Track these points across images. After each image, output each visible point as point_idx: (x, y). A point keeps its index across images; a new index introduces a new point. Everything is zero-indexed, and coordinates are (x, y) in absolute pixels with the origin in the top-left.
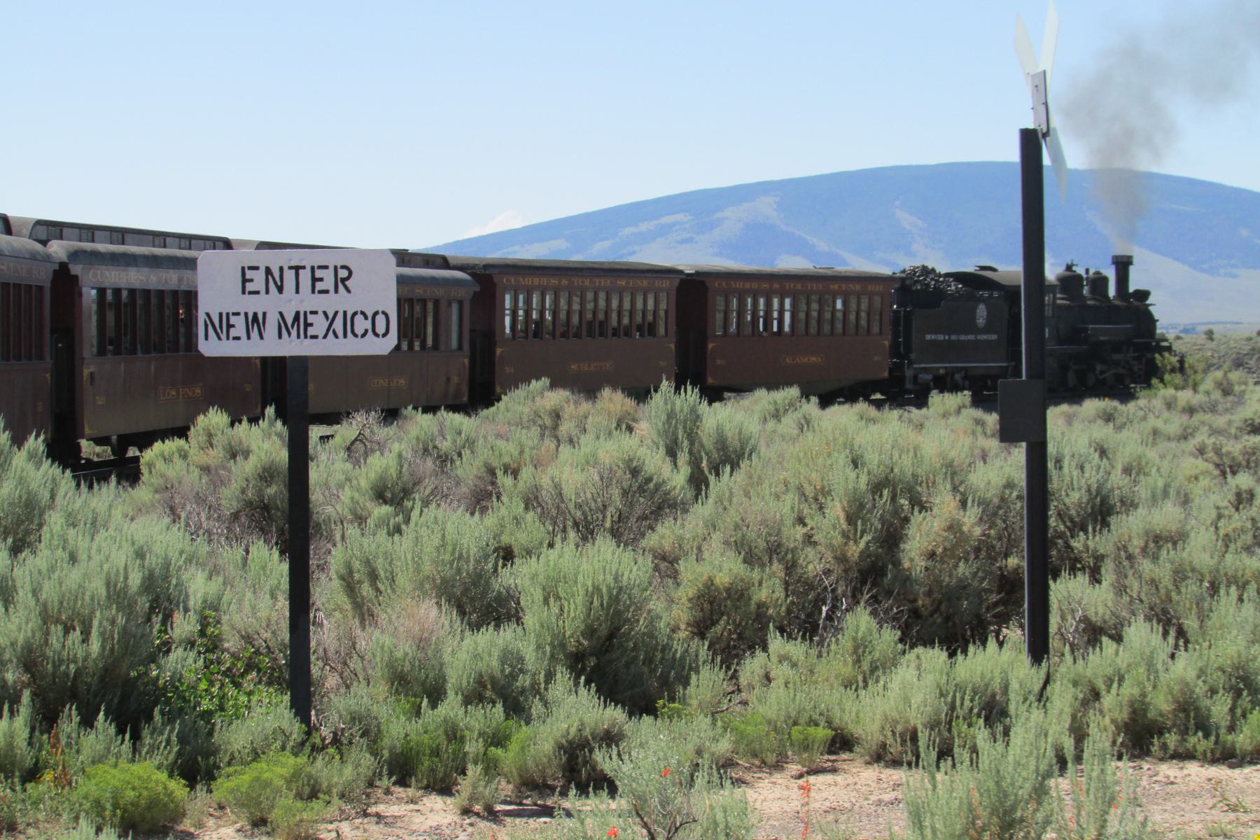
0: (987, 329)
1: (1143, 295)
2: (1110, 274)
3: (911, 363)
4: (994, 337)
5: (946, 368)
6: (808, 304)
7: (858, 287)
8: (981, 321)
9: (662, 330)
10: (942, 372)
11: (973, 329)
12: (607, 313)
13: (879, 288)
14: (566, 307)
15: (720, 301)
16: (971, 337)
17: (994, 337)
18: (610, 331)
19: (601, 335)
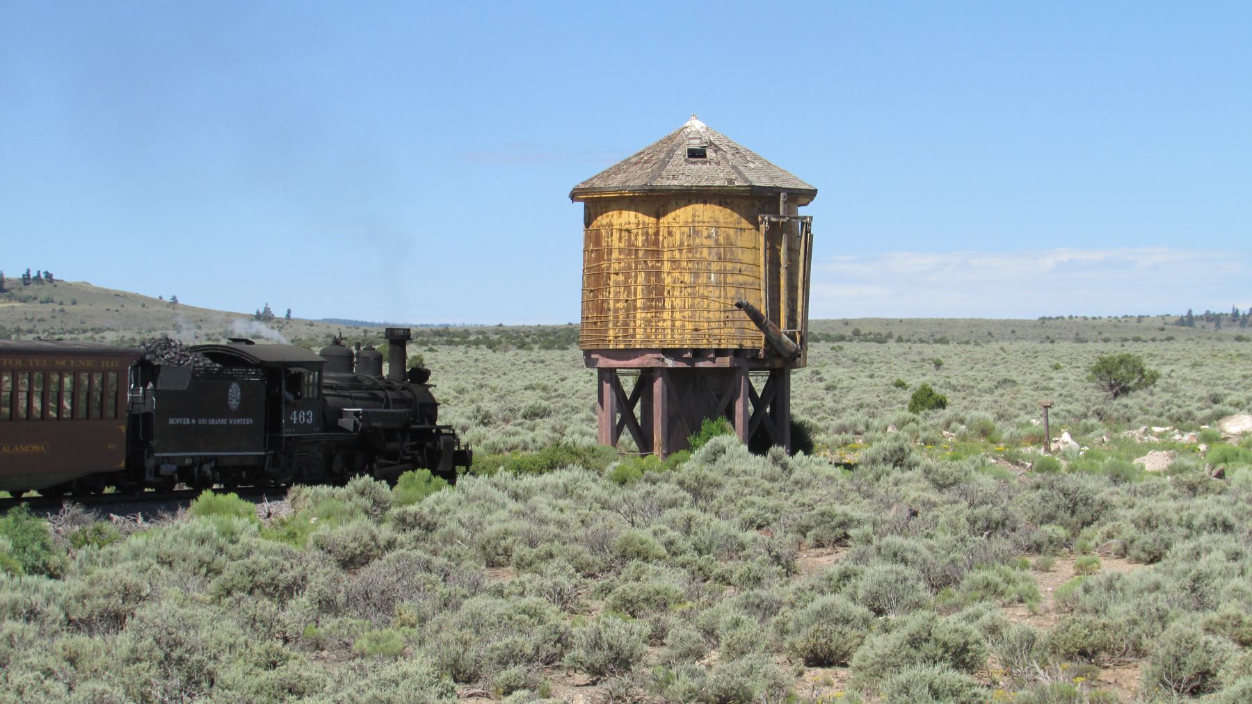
0: (241, 412)
4: (249, 421)
8: (234, 403)
10: (188, 462)
11: (224, 411)
16: (224, 421)
17: (249, 421)
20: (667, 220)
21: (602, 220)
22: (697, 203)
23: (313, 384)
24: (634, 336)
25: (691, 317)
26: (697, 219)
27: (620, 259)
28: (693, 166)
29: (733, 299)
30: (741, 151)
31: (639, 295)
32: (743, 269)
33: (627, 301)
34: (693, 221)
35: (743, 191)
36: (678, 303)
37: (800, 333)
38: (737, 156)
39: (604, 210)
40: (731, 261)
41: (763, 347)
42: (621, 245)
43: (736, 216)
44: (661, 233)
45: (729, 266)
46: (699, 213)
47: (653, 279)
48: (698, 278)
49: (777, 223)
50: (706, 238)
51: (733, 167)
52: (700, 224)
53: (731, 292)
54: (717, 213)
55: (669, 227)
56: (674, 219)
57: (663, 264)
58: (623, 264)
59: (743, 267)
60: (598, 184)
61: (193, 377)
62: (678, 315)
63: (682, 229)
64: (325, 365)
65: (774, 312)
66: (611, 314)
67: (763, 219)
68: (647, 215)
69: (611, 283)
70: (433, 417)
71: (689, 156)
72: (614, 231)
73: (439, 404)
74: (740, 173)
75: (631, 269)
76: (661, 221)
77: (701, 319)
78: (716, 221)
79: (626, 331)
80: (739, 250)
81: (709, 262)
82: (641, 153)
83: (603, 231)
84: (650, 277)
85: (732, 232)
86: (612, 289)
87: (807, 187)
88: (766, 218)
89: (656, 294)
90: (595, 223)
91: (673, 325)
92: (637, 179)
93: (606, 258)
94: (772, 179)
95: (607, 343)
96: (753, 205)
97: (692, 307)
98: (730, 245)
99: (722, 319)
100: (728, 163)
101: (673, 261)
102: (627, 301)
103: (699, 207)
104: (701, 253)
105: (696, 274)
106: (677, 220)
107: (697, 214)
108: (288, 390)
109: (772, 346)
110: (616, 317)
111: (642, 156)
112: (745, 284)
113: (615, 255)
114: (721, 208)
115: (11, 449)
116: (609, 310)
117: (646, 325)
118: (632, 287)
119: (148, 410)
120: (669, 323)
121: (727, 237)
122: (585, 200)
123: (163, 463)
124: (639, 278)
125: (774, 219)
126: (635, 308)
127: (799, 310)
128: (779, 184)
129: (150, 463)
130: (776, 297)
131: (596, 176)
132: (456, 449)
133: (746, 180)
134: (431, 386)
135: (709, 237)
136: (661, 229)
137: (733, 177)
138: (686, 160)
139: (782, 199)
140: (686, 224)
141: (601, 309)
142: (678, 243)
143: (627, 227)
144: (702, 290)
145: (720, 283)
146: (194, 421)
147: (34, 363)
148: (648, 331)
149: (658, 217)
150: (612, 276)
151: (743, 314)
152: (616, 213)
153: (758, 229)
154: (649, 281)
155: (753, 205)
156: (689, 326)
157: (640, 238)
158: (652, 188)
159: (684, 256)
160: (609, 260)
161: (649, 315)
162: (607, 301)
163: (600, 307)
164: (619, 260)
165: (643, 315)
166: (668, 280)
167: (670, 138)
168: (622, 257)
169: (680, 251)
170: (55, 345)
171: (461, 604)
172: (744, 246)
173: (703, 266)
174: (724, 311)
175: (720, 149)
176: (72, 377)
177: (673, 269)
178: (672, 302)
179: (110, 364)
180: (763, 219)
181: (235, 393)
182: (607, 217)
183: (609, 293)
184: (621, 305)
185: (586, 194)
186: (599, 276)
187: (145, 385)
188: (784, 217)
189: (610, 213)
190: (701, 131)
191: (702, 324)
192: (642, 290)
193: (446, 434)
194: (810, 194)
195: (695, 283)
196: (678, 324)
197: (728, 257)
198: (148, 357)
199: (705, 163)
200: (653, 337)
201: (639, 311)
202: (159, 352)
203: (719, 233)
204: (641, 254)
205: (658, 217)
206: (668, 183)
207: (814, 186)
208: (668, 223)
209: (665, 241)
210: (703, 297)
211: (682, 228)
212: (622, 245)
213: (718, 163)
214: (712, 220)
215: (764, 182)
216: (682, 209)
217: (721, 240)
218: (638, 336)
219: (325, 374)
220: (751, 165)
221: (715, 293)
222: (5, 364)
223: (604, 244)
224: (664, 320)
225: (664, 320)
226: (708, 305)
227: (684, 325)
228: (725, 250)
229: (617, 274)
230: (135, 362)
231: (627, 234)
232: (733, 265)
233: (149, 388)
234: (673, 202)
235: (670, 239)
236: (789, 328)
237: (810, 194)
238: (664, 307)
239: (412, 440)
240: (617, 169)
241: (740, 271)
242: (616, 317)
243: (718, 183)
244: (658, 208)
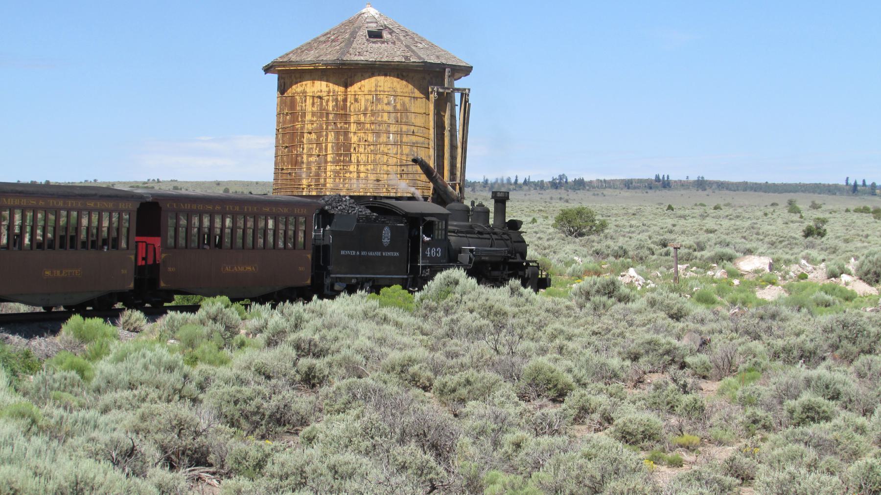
0: (391, 248)
1: (515, 225)
2: (490, 205)
3: (329, 273)
4: (396, 254)
5: (357, 278)
6: (286, 225)
7: (286, 210)
8: (386, 241)
9: (124, 245)
10: (353, 281)
11: (379, 247)
12: (118, 230)
13: (304, 211)
14: (197, 224)
15: (171, 222)
16: (379, 254)
17: (396, 254)
18: (79, 245)
19: (72, 247)
20: (355, 88)
21: (297, 88)
22: (379, 75)
23: (442, 230)
24: (325, 185)
25: (374, 170)
26: (379, 89)
27: (313, 121)
28: (374, 45)
29: (407, 155)
30: (409, 33)
31: (330, 151)
32: (415, 131)
33: (319, 156)
34: (376, 91)
35: (417, 66)
36: (363, 158)
37: (459, 184)
38: (408, 37)
39: (299, 80)
40: (407, 124)
41: (431, 196)
42: (314, 109)
43: (411, 87)
44: (349, 100)
45: (405, 128)
46: (381, 84)
47: (342, 138)
48: (380, 137)
49: (443, 93)
50: (386, 104)
51: (407, 46)
52: (382, 93)
53: (406, 150)
54: (395, 84)
55: (355, 95)
56: (360, 88)
57: (350, 125)
58: (315, 125)
59: (416, 129)
60: (294, 58)
61: (358, 221)
62: (362, 168)
63: (367, 97)
64: (450, 216)
65: (440, 166)
66: (305, 166)
67: (433, 90)
68: (336, 84)
69: (305, 141)
70: (523, 254)
71: (370, 37)
72: (308, 97)
73: (528, 245)
74: (413, 51)
75: (322, 129)
76: (349, 90)
77: (382, 172)
78: (394, 91)
79: (318, 180)
80: (413, 115)
81: (389, 125)
82: (327, 34)
83: (298, 98)
84: (338, 137)
85: (407, 100)
86: (305, 146)
87: (464, 64)
88: (435, 89)
89: (344, 150)
90: (290, 90)
91: (358, 177)
92: (329, 55)
93: (300, 120)
94: (438, 57)
95: (301, 190)
96: (424, 78)
97: (374, 162)
98: (405, 111)
99: (399, 172)
100: (402, 43)
101: (358, 123)
102: (319, 156)
103: (381, 79)
104: (382, 117)
105: (377, 134)
106: (363, 89)
107: (379, 84)
108: (424, 233)
109: (439, 195)
110: (309, 169)
111: (329, 36)
112: (417, 143)
113: (308, 117)
114: (399, 80)
115: (231, 269)
116: (303, 163)
117: (335, 176)
118: (324, 145)
119: (326, 242)
120: (355, 175)
121: (403, 104)
122: (279, 72)
123: (337, 282)
124: (330, 137)
125: (441, 90)
126: (326, 162)
127: (459, 165)
128: (444, 62)
129: (327, 281)
130: (441, 154)
131: (292, 52)
132: (540, 276)
133: (419, 57)
134: (523, 232)
135: (388, 104)
136: (349, 96)
137: (408, 54)
138: (367, 40)
139: (446, 74)
140: (370, 93)
141: (296, 162)
142: (363, 108)
143: (319, 94)
144: (383, 148)
145: (397, 142)
146: (358, 253)
147: (248, 209)
148: (337, 180)
149: (346, 86)
150: (305, 135)
151: (418, 168)
152: (309, 83)
153: (428, 98)
154: (338, 139)
155: (424, 78)
156: (372, 177)
157: (331, 104)
158: (343, 62)
159: (368, 119)
160: (303, 121)
161: (338, 168)
162: (301, 155)
163: (294, 160)
164: (312, 122)
165: (333, 168)
166: (354, 139)
167: (351, 22)
168: (315, 119)
169: (365, 114)
170: (263, 197)
171: (110, 410)
172: (418, 112)
173: (383, 127)
174: (401, 165)
175: (393, 32)
176: (44, 212)
177: (359, 130)
178: (358, 157)
179: (300, 211)
180: (433, 90)
181: (387, 233)
182: (301, 86)
183: (303, 149)
184: (312, 159)
185: (284, 66)
186: (293, 135)
187: (324, 227)
188: (448, 89)
189: (304, 83)
190: (376, 16)
191: (382, 176)
192: (332, 147)
193: (533, 266)
194: (466, 70)
195: (376, 141)
196: (362, 175)
197: (404, 121)
198: (327, 208)
199: (383, 42)
200: (341, 186)
201: (329, 164)
202: (334, 204)
203: (397, 100)
204: (331, 117)
205: (346, 86)
206: (356, 58)
207: (470, 64)
208: (355, 92)
209: (352, 107)
210: (384, 154)
211: (366, 96)
212: (315, 109)
213: (394, 43)
214: (391, 90)
215: (433, 60)
216: (367, 81)
217: (399, 107)
218: (328, 185)
219: (450, 223)
220: (419, 45)
221: (393, 150)
222: (51, 204)
223: (298, 108)
224: (351, 172)
225: (351, 172)
226: (387, 161)
227: (367, 177)
228: (402, 114)
229: (310, 133)
230: (317, 212)
231: (319, 100)
232: (409, 127)
233: (327, 229)
234: (359, 75)
235: (357, 105)
236: (451, 181)
237: (466, 70)
238: (350, 161)
239: (509, 270)
240: (309, 46)
241: (413, 132)
242: (309, 169)
243: (396, 59)
244: (347, 79)
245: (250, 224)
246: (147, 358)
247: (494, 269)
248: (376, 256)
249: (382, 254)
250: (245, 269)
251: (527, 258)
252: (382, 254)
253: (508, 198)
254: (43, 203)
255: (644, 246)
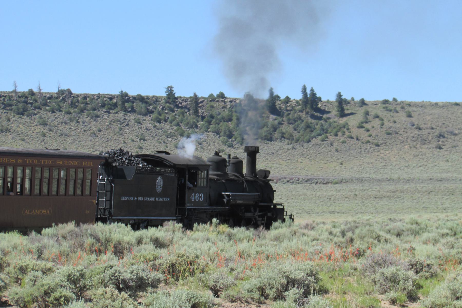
2: (243, 156)
4: (167, 199)
5: (134, 220)
8: (159, 189)
11: (153, 193)
16: (153, 199)
17: (167, 199)
115: (30, 212)
146: (136, 199)
176: (4, 168)
179: (88, 164)
181: (160, 181)
245: (46, 174)
246: (198, 261)
247: (248, 211)
248: (150, 201)
249: (155, 199)
250: (41, 212)
251: (275, 202)
252: (155, 199)
253: (258, 152)
254: (21, 161)
255: (397, 191)
